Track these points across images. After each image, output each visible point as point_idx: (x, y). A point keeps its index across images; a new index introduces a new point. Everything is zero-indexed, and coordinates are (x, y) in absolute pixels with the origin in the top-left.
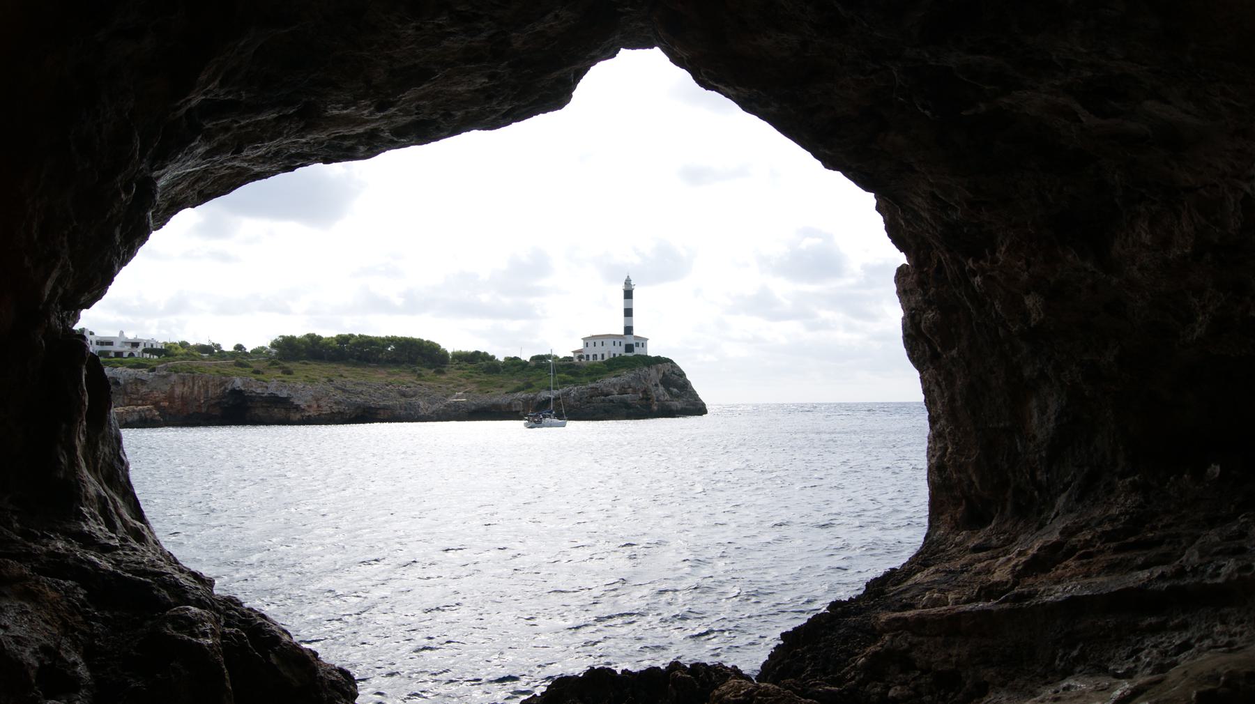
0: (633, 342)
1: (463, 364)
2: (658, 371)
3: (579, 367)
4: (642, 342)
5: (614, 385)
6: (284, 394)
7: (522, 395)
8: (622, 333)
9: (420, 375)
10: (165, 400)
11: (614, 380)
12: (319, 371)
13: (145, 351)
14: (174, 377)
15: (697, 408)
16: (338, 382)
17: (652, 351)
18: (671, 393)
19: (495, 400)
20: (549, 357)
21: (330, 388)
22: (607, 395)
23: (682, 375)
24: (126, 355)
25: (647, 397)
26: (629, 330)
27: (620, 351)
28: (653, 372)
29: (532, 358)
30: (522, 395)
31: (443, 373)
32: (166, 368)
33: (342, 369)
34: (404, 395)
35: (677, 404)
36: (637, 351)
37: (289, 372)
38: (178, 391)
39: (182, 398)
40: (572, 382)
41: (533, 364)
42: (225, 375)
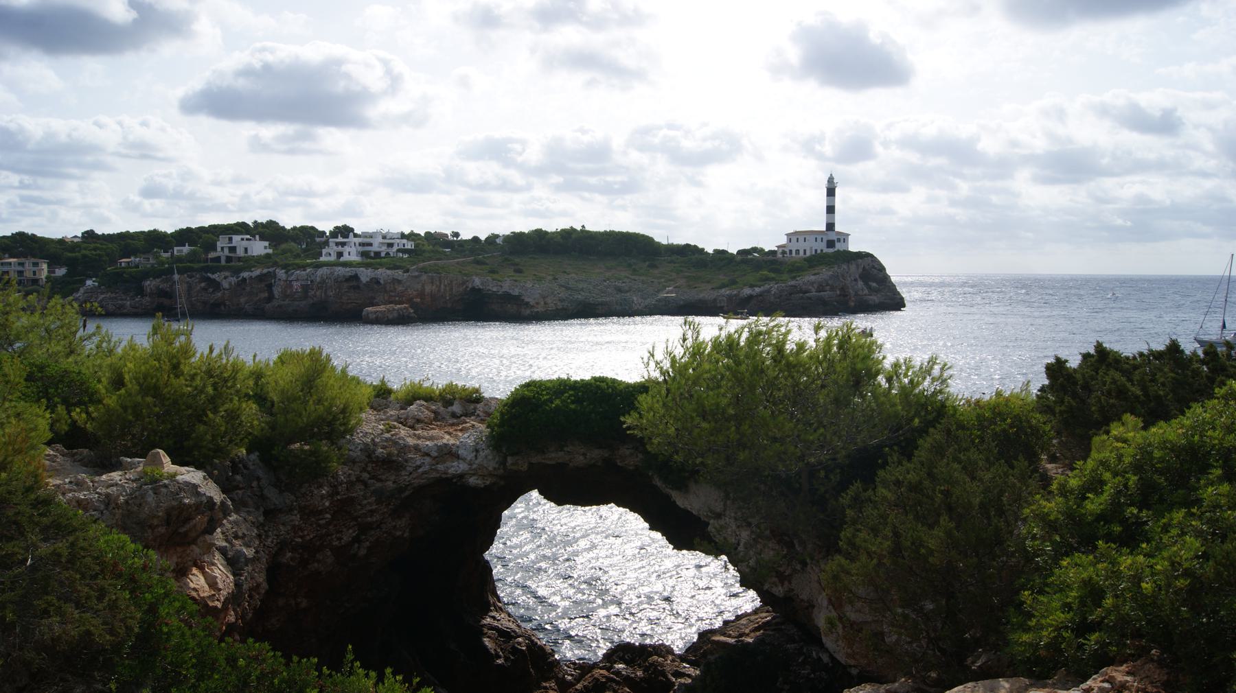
0: (835, 238)
1: (674, 257)
2: (858, 266)
3: (781, 263)
4: (844, 237)
5: (812, 283)
6: (516, 292)
7: (726, 292)
8: (824, 228)
9: (634, 270)
11: (813, 278)
13: (399, 251)
14: (424, 277)
17: (853, 247)
18: (869, 288)
19: (701, 296)
20: (755, 250)
22: (806, 292)
24: (383, 255)
26: (830, 226)
27: (821, 246)
28: (853, 267)
29: (740, 252)
30: (726, 292)
34: (619, 290)
35: (875, 299)
37: (519, 271)
38: (428, 289)
40: (773, 279)
41: (739, 258)
42: (466, 275)
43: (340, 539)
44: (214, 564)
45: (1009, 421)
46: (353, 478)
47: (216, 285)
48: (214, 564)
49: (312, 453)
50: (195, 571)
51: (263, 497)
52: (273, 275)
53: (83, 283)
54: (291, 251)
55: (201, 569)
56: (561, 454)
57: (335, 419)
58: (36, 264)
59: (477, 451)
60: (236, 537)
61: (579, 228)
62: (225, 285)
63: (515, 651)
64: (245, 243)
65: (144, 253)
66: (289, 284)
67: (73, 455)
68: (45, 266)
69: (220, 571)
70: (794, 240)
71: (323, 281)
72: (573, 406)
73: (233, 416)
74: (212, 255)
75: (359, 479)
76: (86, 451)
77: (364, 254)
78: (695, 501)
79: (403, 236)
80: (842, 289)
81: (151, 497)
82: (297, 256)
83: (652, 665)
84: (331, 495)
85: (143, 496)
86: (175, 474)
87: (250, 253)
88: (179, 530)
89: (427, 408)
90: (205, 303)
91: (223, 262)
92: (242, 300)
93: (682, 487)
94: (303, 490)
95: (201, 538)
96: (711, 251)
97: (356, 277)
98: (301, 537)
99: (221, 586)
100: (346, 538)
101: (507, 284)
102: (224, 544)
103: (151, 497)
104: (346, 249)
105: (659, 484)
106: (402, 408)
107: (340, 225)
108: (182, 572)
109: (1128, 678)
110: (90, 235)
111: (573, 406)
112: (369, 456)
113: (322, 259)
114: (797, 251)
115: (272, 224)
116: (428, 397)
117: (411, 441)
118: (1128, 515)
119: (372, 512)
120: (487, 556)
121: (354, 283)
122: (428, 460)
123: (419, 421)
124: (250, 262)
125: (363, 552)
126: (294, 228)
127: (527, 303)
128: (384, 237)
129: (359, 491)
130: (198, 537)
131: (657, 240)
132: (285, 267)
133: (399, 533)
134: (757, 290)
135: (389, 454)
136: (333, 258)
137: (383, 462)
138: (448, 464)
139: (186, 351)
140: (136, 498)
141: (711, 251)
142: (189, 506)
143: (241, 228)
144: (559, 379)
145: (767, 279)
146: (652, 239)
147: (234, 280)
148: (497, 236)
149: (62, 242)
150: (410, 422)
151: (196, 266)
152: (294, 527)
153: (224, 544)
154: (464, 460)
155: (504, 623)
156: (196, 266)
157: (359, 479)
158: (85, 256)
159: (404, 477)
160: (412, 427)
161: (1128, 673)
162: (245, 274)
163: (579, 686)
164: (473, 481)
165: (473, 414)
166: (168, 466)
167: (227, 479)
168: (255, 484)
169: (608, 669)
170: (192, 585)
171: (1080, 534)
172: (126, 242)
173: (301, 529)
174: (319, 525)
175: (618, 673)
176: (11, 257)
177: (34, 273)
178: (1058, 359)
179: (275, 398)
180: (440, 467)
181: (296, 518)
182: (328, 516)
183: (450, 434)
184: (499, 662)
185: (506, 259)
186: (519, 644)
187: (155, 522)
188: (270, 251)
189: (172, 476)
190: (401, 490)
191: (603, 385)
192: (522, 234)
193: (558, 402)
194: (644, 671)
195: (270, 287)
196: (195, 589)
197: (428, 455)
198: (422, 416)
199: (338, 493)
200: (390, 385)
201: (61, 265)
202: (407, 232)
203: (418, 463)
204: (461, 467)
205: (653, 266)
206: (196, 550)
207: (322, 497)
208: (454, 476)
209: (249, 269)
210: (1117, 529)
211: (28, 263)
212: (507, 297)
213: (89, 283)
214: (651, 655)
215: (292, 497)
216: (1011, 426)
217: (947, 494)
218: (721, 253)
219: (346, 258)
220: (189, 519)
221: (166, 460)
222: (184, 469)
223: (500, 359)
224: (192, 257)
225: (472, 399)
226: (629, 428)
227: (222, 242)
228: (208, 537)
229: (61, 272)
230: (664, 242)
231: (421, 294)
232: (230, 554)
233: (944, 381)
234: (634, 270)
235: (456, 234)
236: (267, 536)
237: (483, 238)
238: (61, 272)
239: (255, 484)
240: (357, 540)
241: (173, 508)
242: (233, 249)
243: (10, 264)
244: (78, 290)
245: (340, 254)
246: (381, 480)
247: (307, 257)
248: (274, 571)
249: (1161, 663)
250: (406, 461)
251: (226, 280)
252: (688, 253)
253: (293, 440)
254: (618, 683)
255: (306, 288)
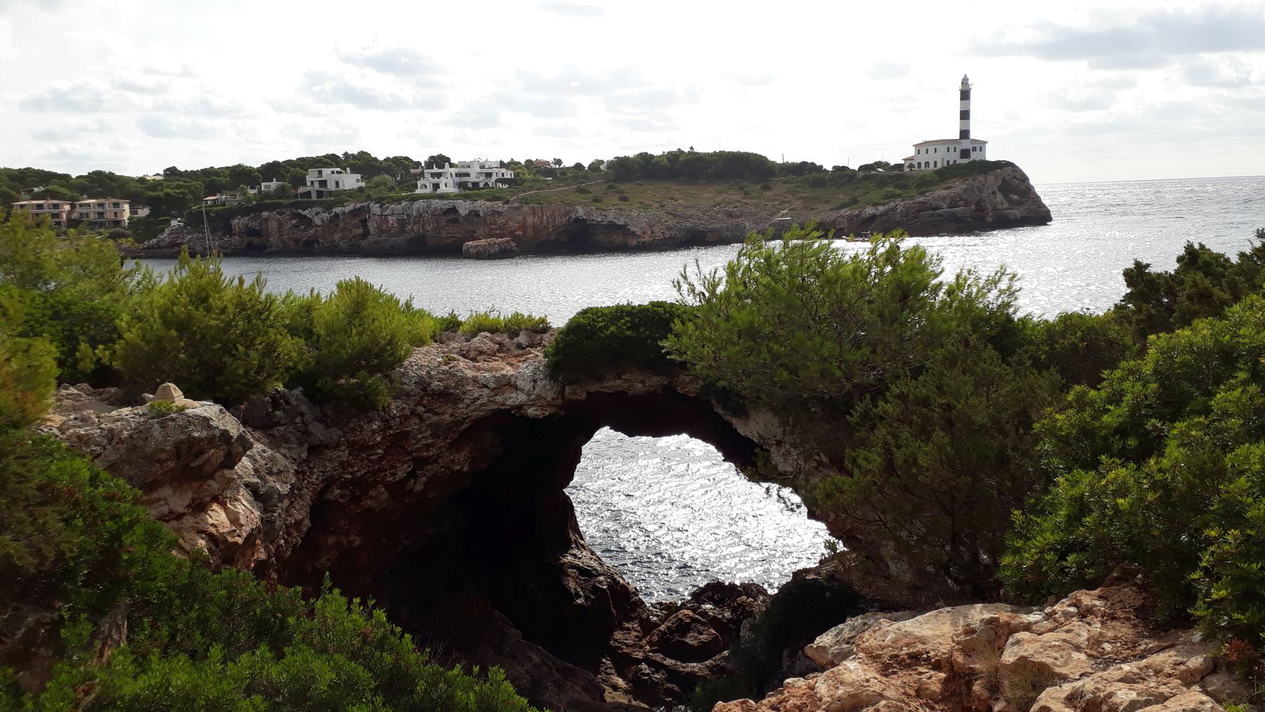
0: (970, 147)
1: (790, 177)
3: (908, 177)
4: (980, 145)
5: (944, 199)
6: (621, 222)
7: (846, 212)
8: (956, 135)
9: (746, 193)
10: (519, 229)
12: (651, 192)
13: (497, 181)
14: (526, 208)
15: (1039, 216)
16: (670, 205)
17: (991, 155)
20: (879, 164)
21: (661, 213)
23: (1025, 179)
24: (481, 185)
25: (980, 208)
26: (965, 134)
27: (954, 157)
28: (991, 178)
29: (861, 168)
31: (770, 189)
32: (517, 200)
33: (675, 189)
34: (730, 215)
35: (1016, 212)
36: (975, 156)
37: (624, 199)
38: (530, 220)
39: (534, 227)
40: (899, 196)
41: (862, 174)
42: (568, 204)
43: (394, 474)
44: (237, 500)
45: (1079, 334)
46: (407, 412)
47: (308, 222)
48: (237, 500)
49: (360, 386)
50: (215, 506)
51: (307, 433)
52: (366, 210)
53: (167, 222)
54: (385, 184)
55: (223, 505)
56: (618, 382)
57: (383, 350)
58: (116, 205)
59: (535, 381)
60: (270, 473)
61: (686, 150)
62: (317, 221)
63: (595, 589)
64: (336, 175)
65: (231, 190)
66: (384, 218)
67: (101, 394)
68: (126, 207)
69: (246, 508)
70: (923, 150)
71: (420, 215)
72: (629, 333)
73: (270, 349)
74: (301, 190)
75: (413, 413)
76: (113, 390)
77: (462, 185)
78: (752, 428)
79: (502, 165)
80: (978, 203)
81: (157, 431)
82: (392, 189)
83: (739, 605)
84: (382, 430)
85: (149, 430)
86: (184, 408)
87: (341, 187)
88: (196, 467)
89: (492, 340)
90: (297, 241)
91: (314, 197)
92: (336, 237)
93: (742, 413)
94: (351, 425)
95: (220, 473)
96: (829, 168)
97: (454, 210)
98: (351, 473)
99: (242, 521)
100: (401, 474)
101: (612, 213)
102: (256, 480)
103: (157, 431)
104: (442, 181)
105: (720, 412)
106: (468, 340)
107: (435, 154)
108: (200, 507)
109: (1097, 603)
110: (172, 172)
111: (629, 333)
112: (424, 389)
113: (417, 191)
114: (927, 164)
115: (363, 155)
116: (494, 329)
117: (470, 373)
118: (1149, 427)
119: (428, 446)
120: (566, 491)
121: (452, 216)
122: (486, 391)
123: (481, 353)
124: (341, 196)
125: (419, 487)
126: (387, 159)
127: (634, 233)
128: (482, 167)
129: (413, 425)
130: (216, 471)
131: (771, 158)
132: (379, 200)
133: (457, 468)
134: (880, 208)
135: (446, 387)
136: (429, 190)
137: (441, 394)
138: (507, 395)
139: (216, 285)
140: (142, 432)
141: (829, 168)
142: (200, 439)
143: (331, 160)
144: (618, 306)
145: (892, 196)
146: (765, 158)
147: (326, 216)
148: (602, 162)
149: (142, 180)
150: (472, 354)
151: (285, 202)
152: (341, 463)
153: (256, 480)
154: (522, 390)
155: (585, 559)
156: (285, 202)
157: (413, 413)
158: (167, 195)
159: (462, 410)
160: (474, 360)
161: (1100, 597)
162: (338, 210)
163: (662, 628)
164: (531, 412)
165: (539, 344)
166: (179, 397)
167: (267, 415)
168: (298, 420)
169: (694, 610)
170: (210, 521)
171: (1086, 449)
172: (211, 179)
173: (352, 466)
174: (370, 461)
175: (704, 614)
176: (90, 198)
177: (116, 214)
178: (1138, 264)
179: (322, 332)
180: (499, 399)
181: (344, 454)
182: (380, 451)
183: (512, 365)
184: (579, 601)
185: (611, 187)
186: (600, 582)
187: (163, 456)
188: (363, 184)
189: (181, 410)
190: (459, 423)
191: (661, 310)
192: (626, 158)
193: (613, 328)
194: (733, 612)
195: (364, 222)
196: (212, 525)
197: (486, 386)
198: (485, 348)
199: (390, 428)
200: (460, 319)
201: (144, 205)
202: (506, 161)
203: (476, 395)
204: (521, 398)
205: (766, 188)
206: (214, 485)
207: (374, 432)
208: (513, 408)
209: (341, 203)
210: (1132, 442)
211: (108, 202)
212: (613, 227)
213: (174, 223)
214: (740, 594)
215: (340, 432)
216: (1082, 340)
217: (949, 407)
218: (841, 171)
219: (442, 189)
220: (202, 452)
221: (177, 394)
222: (196, 403)
223: (562, 290)
224: (281, 192)
225: (540, 328)
226: (669, 353)
227: (311, 176)
228: (227, 472)
229: (143, 212)
230: (779, 161)
231: (523, 226)
232: (262, 491)
233: (1012, 294)
234: (746, 193)
235: (559, 162)
236: (312, 473)
237: (586, 165)
238: (143, 212)
239: (298, 420)
240: (412, 475)
241: (182, 442)
242: (323, 183)
243: (89, 205)
244: (162, 231)
245: (436, 186)
246: (437, 414)
247: (402, 190)
248: (320, 508)
249: (1142, 588)
250: (464, 393)
251: (319, 217)
252: (805, 172)
253: (343, 375)
254: (703, 624)
255: (402, 223)
